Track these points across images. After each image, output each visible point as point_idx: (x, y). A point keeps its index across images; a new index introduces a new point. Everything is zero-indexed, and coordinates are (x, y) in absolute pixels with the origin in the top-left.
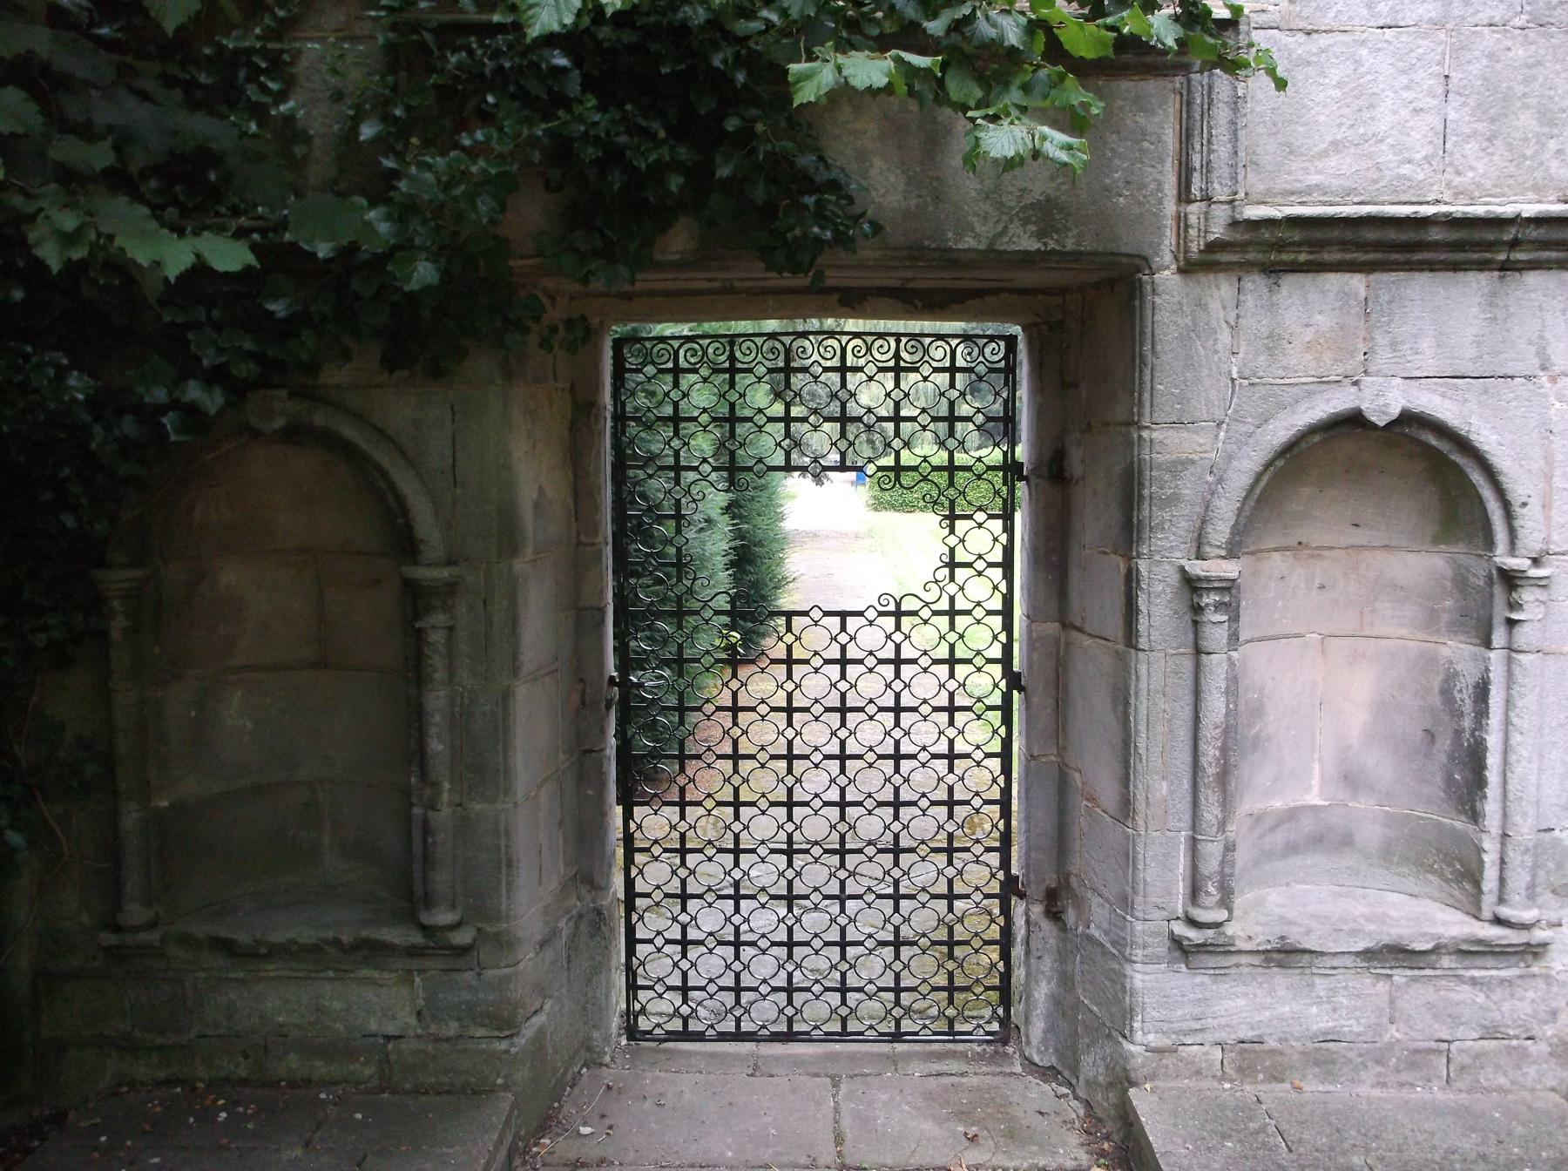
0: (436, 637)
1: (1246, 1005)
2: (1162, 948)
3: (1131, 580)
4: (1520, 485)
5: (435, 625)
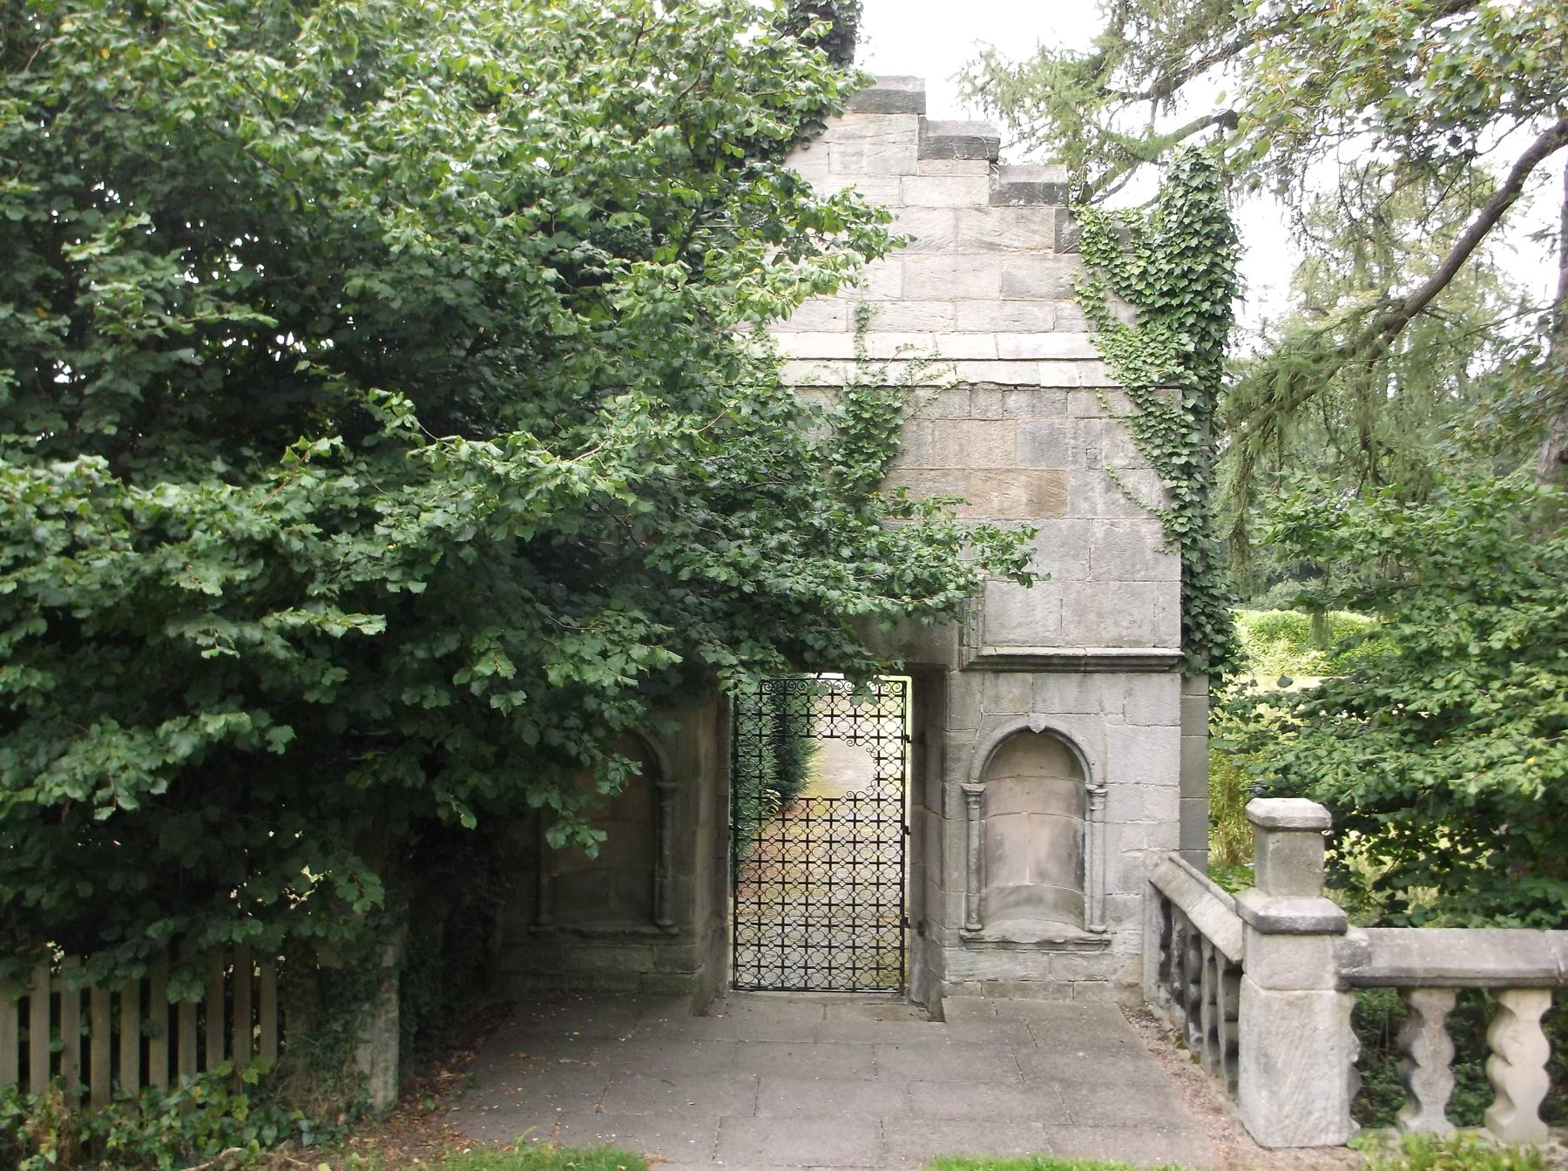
0: (668, 809)
1: (991, 965)
3: (943, 791)
4: (1092, 758)
5: (668, 805)
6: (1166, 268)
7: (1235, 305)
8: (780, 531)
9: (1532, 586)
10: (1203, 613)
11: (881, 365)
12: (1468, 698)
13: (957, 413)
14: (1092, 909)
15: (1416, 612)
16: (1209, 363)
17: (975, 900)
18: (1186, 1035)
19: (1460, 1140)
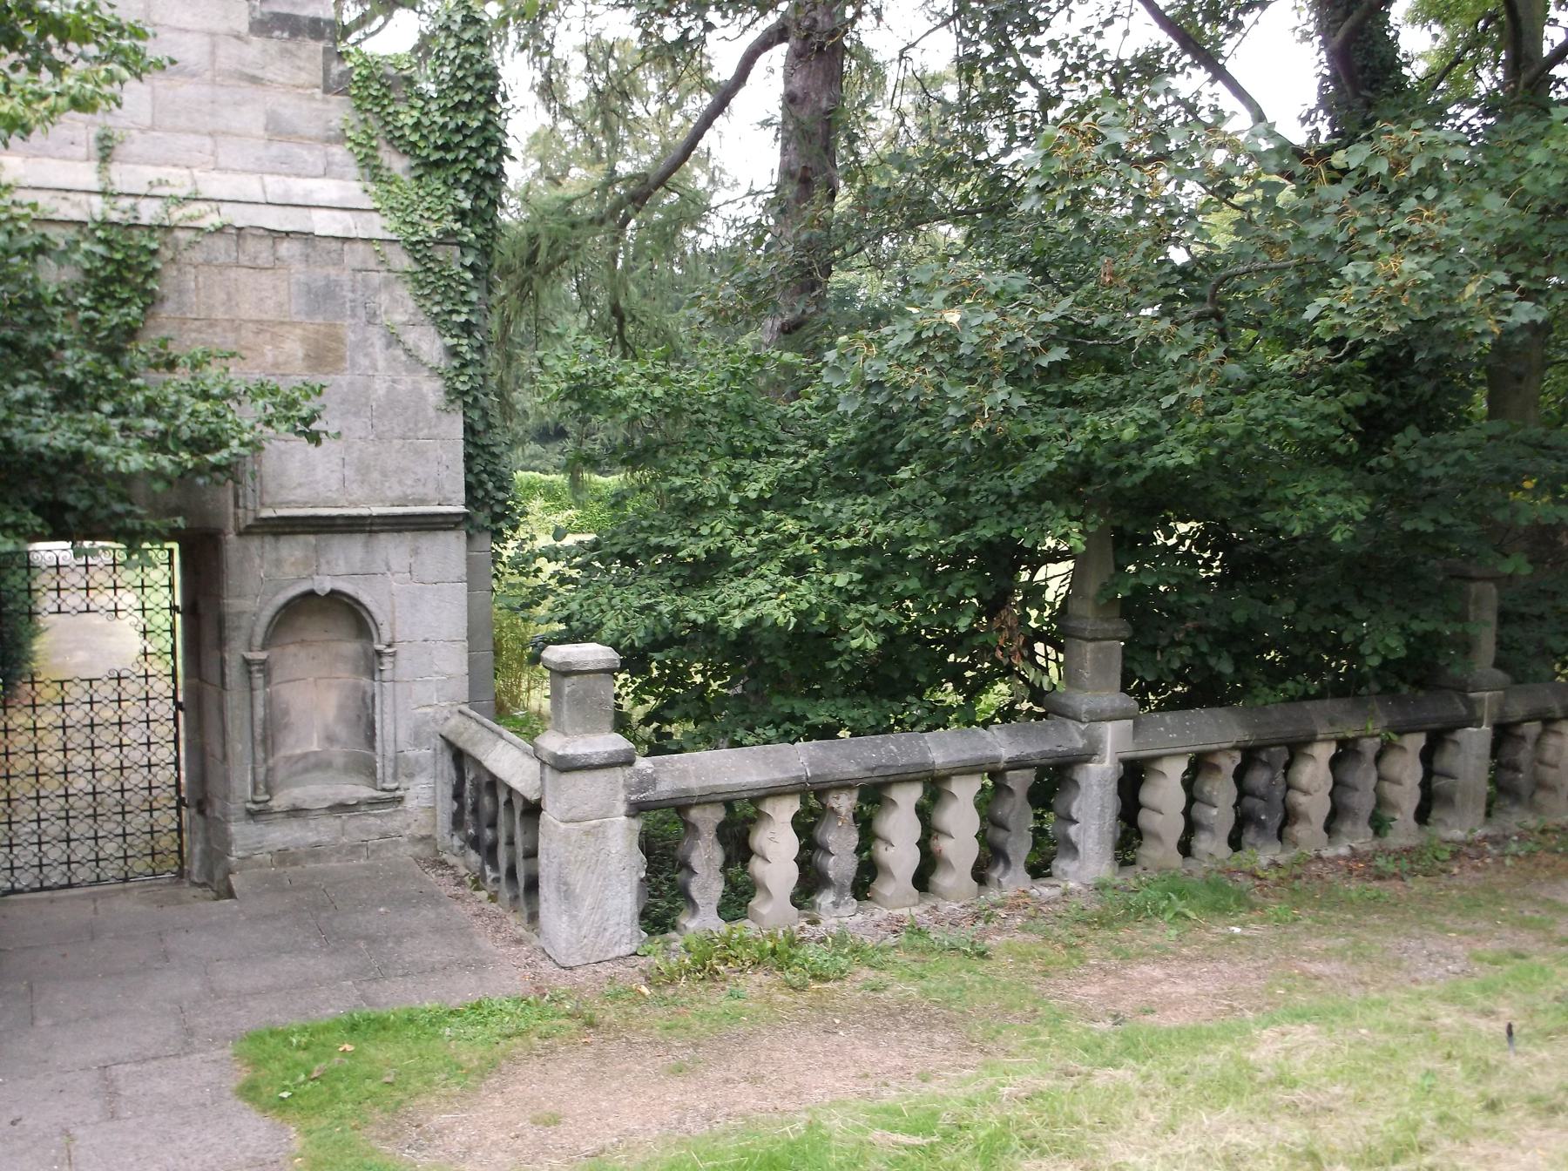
1: (280, 835)
2: (242, 814)
3: (223, 661)
4: (380, 618)
6: (440, 121)
7: (507, 165)
8: (25, 383)
9: (779, 442)
10: (485, 471)
11: (131, 201)
12: (728, 544)
13: (221, 260)
14: (383, 767)
15: (682, 466)
16: (485, 221)
17: (261, 771)
18: (483, 877)
19: (731, 932)
